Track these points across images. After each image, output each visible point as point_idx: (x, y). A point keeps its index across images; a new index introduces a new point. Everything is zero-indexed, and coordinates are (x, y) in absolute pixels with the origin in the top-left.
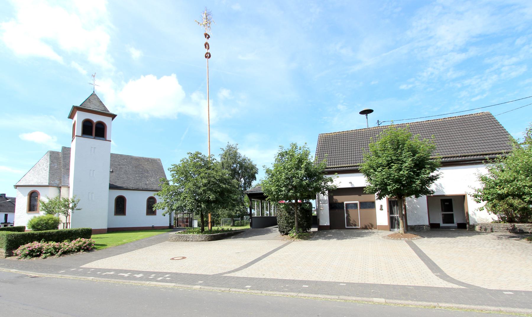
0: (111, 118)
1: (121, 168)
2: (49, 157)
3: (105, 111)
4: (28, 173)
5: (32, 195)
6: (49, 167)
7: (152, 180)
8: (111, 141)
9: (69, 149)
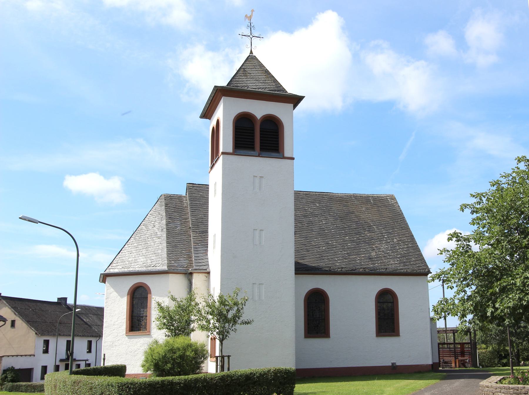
0: (292, 105)
1: (310, 223)
2: (163, 207)
3: (278, 91)
4: (126, 246)
5: (136, 294)
6: (165, 230)
7: (384, 247)
8: (293, 159)
9: (205, 188)
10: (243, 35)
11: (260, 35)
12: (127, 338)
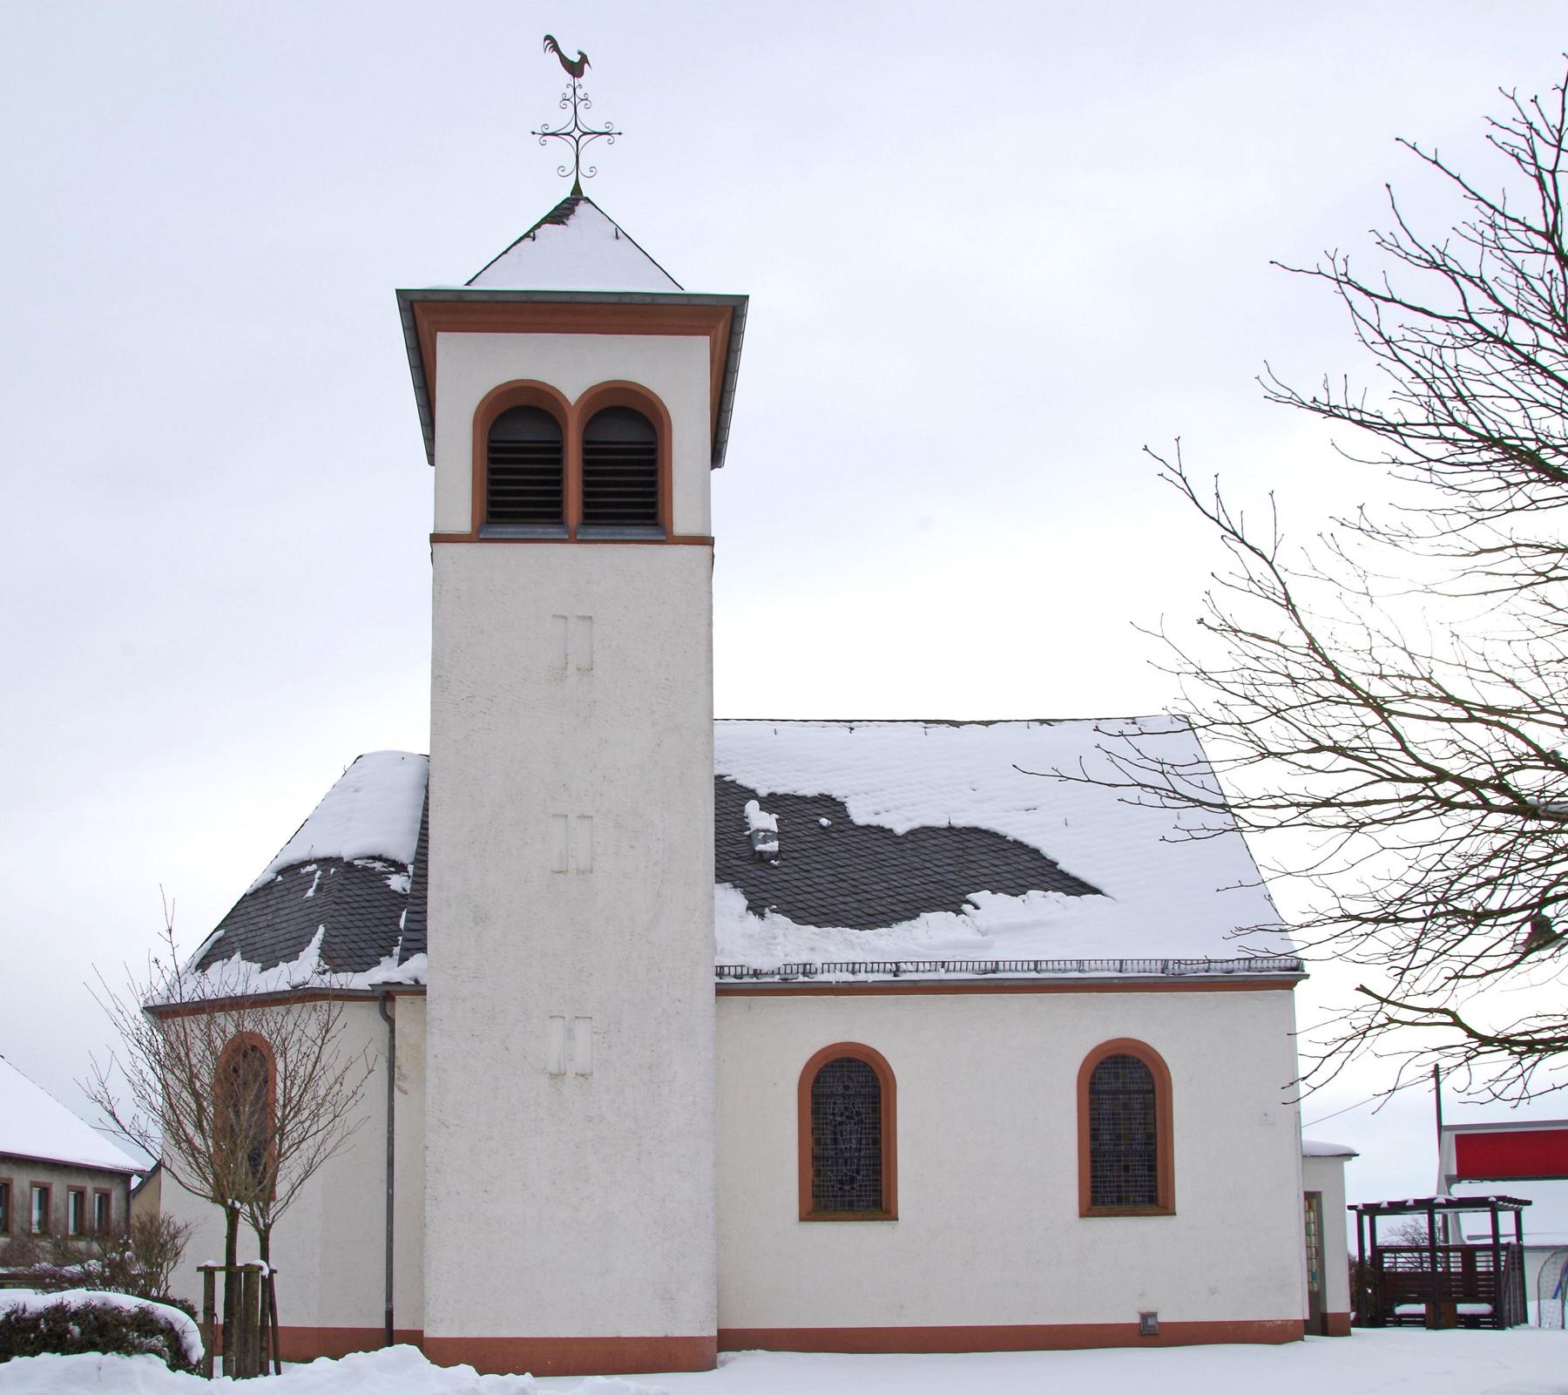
10: (545, 134)
11: (607, 125)
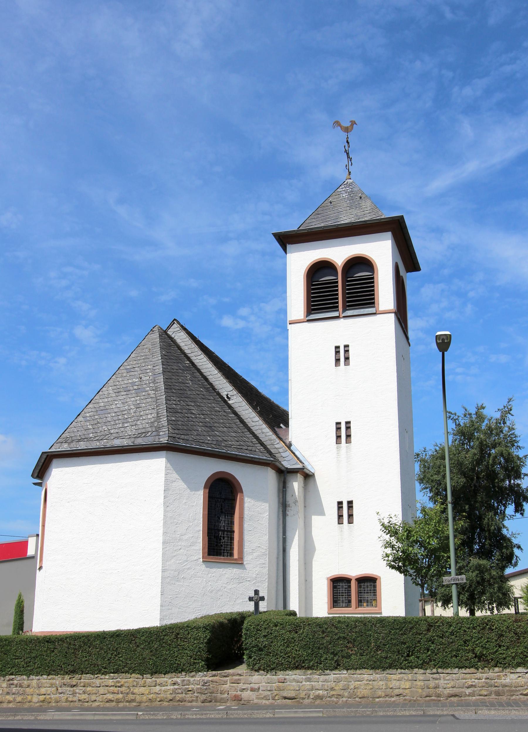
12: (204, 566)
